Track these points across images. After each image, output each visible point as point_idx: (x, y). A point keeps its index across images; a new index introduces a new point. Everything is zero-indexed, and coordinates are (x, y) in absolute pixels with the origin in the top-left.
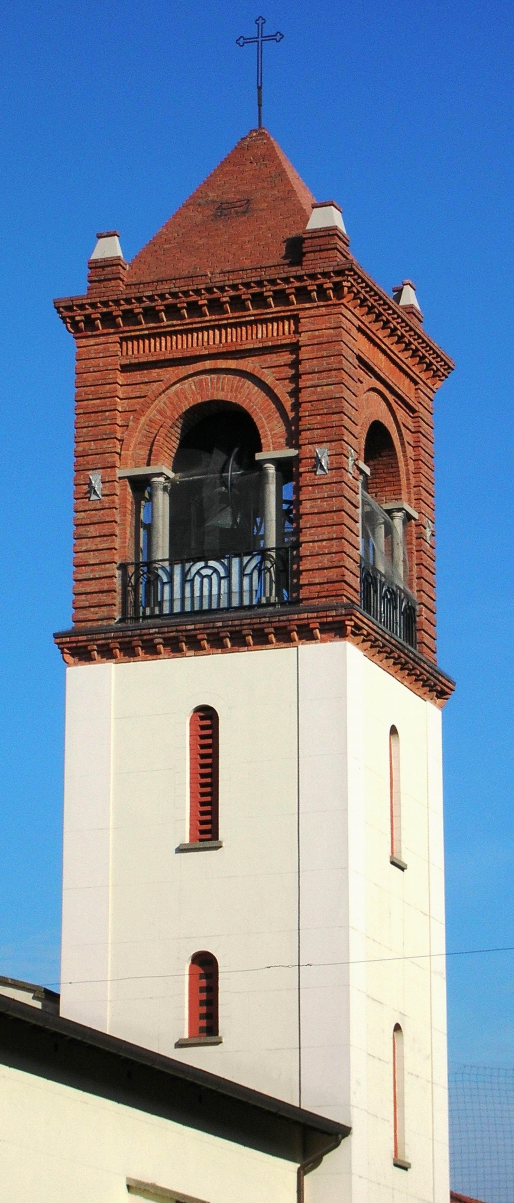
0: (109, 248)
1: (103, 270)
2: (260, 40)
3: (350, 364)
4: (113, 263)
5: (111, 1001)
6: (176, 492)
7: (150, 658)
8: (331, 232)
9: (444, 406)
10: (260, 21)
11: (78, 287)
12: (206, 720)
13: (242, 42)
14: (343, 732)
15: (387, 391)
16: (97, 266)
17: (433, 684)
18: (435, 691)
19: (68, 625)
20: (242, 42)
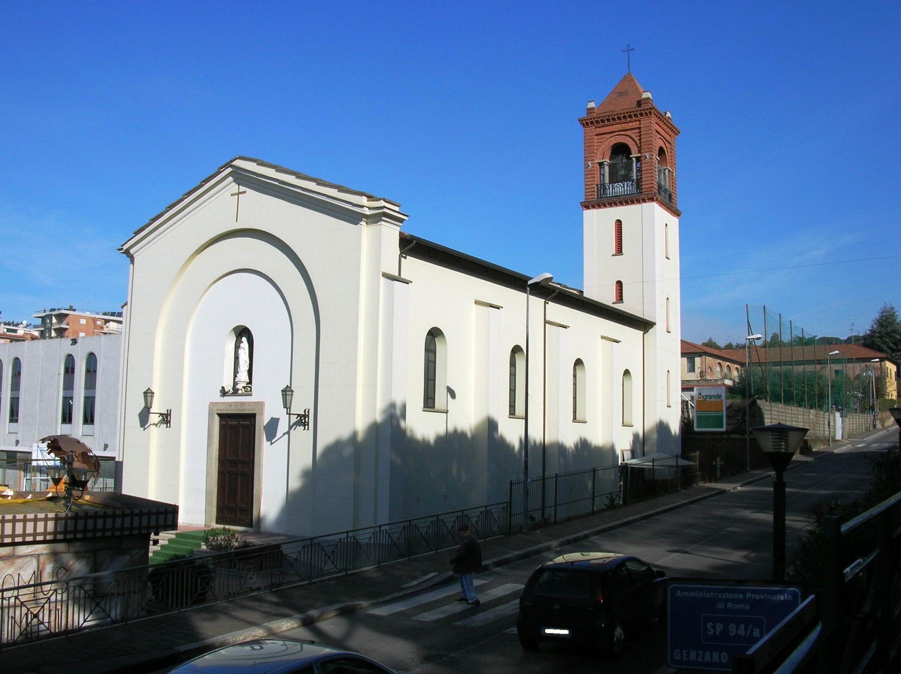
0: (592, 105)
1: (590, 111)
2: (628, 50)
6: (610, 166)
10: (628, 46)
11: (584, 115)
12: (619, 223)
13: (624, 51)
15: (663, 138)
16: (588, 109)
17: (676, 213)
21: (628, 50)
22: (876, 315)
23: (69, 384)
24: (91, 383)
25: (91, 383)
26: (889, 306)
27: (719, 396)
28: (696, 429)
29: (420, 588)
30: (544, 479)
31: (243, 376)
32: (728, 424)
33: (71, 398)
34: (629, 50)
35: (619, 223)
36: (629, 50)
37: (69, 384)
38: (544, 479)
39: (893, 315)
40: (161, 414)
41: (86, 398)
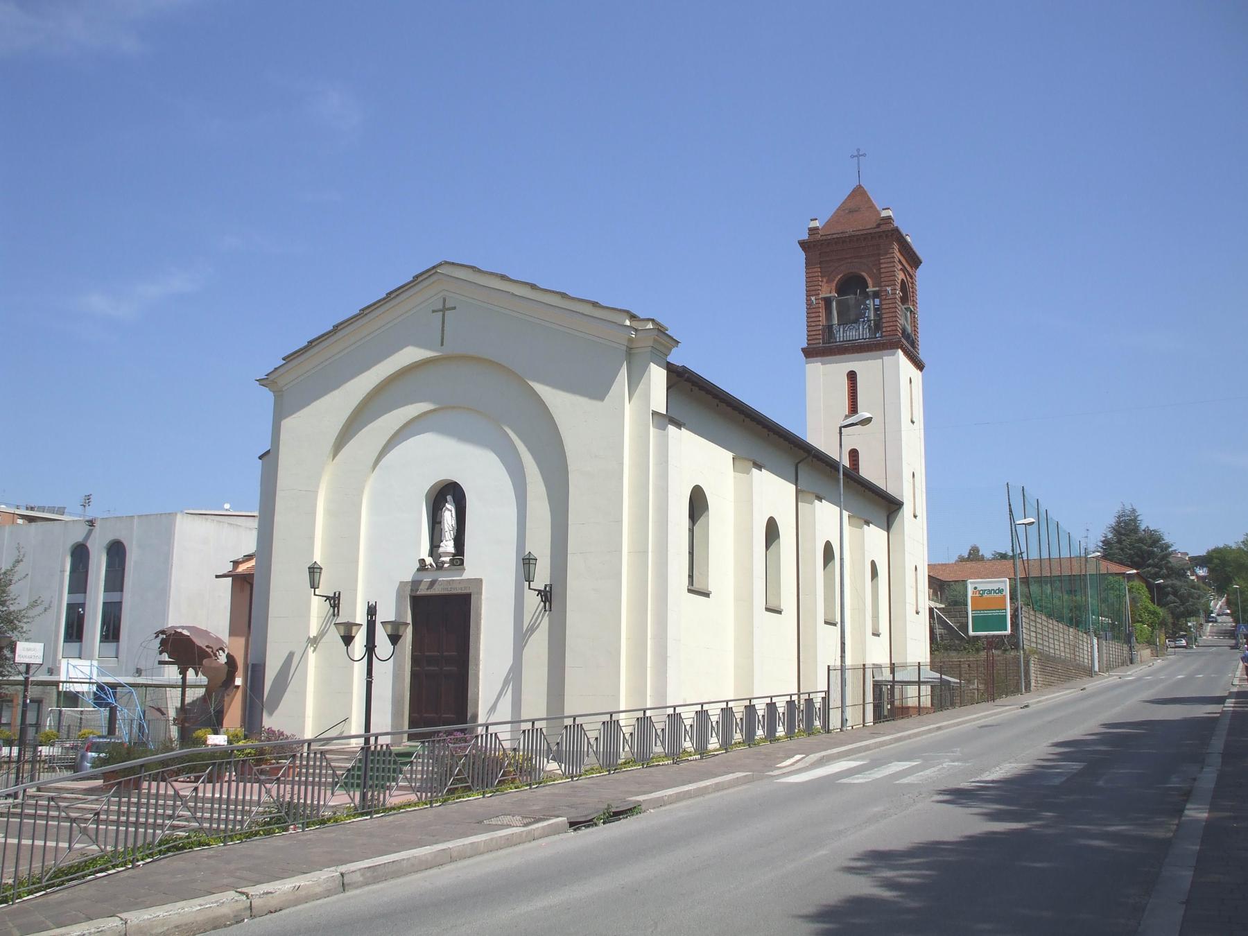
0: (816, 224)
1: (813, 231)
2: (858, 156)
3: (896, 260)
4: (816, 229)
5: (57, 841)
6: (838, 303)
7: (186, 632)
8: (889, 218)
9: (920, 274)
10: (858, 150)
11: (805, 237)
12: (852, 376)
13: (853, 157)
14: (898, 382)
15: (904, 270)
16: (810, 229)
17: (919, 365)
18: (45, 762)
19: (805, 345)
20: (853, 157)
21: (858, 156)
22: (1112, 521)
23: (79, 582)
24: (115, 580)
25: (115, 580)
26: (1129, 507)
27: (1000, 591)
28: (971, 633)
29: (793, 768)
30: (843, 669)
31: (448, 546)
32: (978, 638)
33: (83, 605)
34: (858, 155)
35: (852, 376)
36: (858, 155)
37: (79, 582)
38: (843, 669)
39: (1135, 520)
40: (328, 598)
41: (71, 607)
